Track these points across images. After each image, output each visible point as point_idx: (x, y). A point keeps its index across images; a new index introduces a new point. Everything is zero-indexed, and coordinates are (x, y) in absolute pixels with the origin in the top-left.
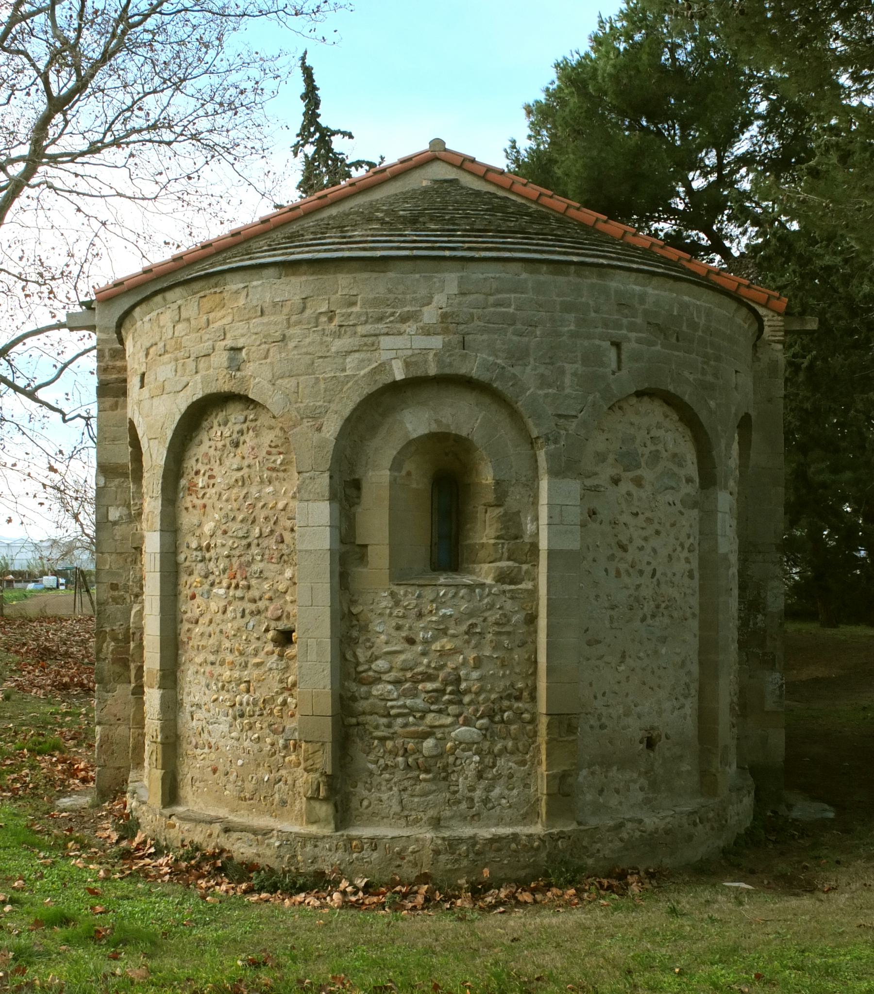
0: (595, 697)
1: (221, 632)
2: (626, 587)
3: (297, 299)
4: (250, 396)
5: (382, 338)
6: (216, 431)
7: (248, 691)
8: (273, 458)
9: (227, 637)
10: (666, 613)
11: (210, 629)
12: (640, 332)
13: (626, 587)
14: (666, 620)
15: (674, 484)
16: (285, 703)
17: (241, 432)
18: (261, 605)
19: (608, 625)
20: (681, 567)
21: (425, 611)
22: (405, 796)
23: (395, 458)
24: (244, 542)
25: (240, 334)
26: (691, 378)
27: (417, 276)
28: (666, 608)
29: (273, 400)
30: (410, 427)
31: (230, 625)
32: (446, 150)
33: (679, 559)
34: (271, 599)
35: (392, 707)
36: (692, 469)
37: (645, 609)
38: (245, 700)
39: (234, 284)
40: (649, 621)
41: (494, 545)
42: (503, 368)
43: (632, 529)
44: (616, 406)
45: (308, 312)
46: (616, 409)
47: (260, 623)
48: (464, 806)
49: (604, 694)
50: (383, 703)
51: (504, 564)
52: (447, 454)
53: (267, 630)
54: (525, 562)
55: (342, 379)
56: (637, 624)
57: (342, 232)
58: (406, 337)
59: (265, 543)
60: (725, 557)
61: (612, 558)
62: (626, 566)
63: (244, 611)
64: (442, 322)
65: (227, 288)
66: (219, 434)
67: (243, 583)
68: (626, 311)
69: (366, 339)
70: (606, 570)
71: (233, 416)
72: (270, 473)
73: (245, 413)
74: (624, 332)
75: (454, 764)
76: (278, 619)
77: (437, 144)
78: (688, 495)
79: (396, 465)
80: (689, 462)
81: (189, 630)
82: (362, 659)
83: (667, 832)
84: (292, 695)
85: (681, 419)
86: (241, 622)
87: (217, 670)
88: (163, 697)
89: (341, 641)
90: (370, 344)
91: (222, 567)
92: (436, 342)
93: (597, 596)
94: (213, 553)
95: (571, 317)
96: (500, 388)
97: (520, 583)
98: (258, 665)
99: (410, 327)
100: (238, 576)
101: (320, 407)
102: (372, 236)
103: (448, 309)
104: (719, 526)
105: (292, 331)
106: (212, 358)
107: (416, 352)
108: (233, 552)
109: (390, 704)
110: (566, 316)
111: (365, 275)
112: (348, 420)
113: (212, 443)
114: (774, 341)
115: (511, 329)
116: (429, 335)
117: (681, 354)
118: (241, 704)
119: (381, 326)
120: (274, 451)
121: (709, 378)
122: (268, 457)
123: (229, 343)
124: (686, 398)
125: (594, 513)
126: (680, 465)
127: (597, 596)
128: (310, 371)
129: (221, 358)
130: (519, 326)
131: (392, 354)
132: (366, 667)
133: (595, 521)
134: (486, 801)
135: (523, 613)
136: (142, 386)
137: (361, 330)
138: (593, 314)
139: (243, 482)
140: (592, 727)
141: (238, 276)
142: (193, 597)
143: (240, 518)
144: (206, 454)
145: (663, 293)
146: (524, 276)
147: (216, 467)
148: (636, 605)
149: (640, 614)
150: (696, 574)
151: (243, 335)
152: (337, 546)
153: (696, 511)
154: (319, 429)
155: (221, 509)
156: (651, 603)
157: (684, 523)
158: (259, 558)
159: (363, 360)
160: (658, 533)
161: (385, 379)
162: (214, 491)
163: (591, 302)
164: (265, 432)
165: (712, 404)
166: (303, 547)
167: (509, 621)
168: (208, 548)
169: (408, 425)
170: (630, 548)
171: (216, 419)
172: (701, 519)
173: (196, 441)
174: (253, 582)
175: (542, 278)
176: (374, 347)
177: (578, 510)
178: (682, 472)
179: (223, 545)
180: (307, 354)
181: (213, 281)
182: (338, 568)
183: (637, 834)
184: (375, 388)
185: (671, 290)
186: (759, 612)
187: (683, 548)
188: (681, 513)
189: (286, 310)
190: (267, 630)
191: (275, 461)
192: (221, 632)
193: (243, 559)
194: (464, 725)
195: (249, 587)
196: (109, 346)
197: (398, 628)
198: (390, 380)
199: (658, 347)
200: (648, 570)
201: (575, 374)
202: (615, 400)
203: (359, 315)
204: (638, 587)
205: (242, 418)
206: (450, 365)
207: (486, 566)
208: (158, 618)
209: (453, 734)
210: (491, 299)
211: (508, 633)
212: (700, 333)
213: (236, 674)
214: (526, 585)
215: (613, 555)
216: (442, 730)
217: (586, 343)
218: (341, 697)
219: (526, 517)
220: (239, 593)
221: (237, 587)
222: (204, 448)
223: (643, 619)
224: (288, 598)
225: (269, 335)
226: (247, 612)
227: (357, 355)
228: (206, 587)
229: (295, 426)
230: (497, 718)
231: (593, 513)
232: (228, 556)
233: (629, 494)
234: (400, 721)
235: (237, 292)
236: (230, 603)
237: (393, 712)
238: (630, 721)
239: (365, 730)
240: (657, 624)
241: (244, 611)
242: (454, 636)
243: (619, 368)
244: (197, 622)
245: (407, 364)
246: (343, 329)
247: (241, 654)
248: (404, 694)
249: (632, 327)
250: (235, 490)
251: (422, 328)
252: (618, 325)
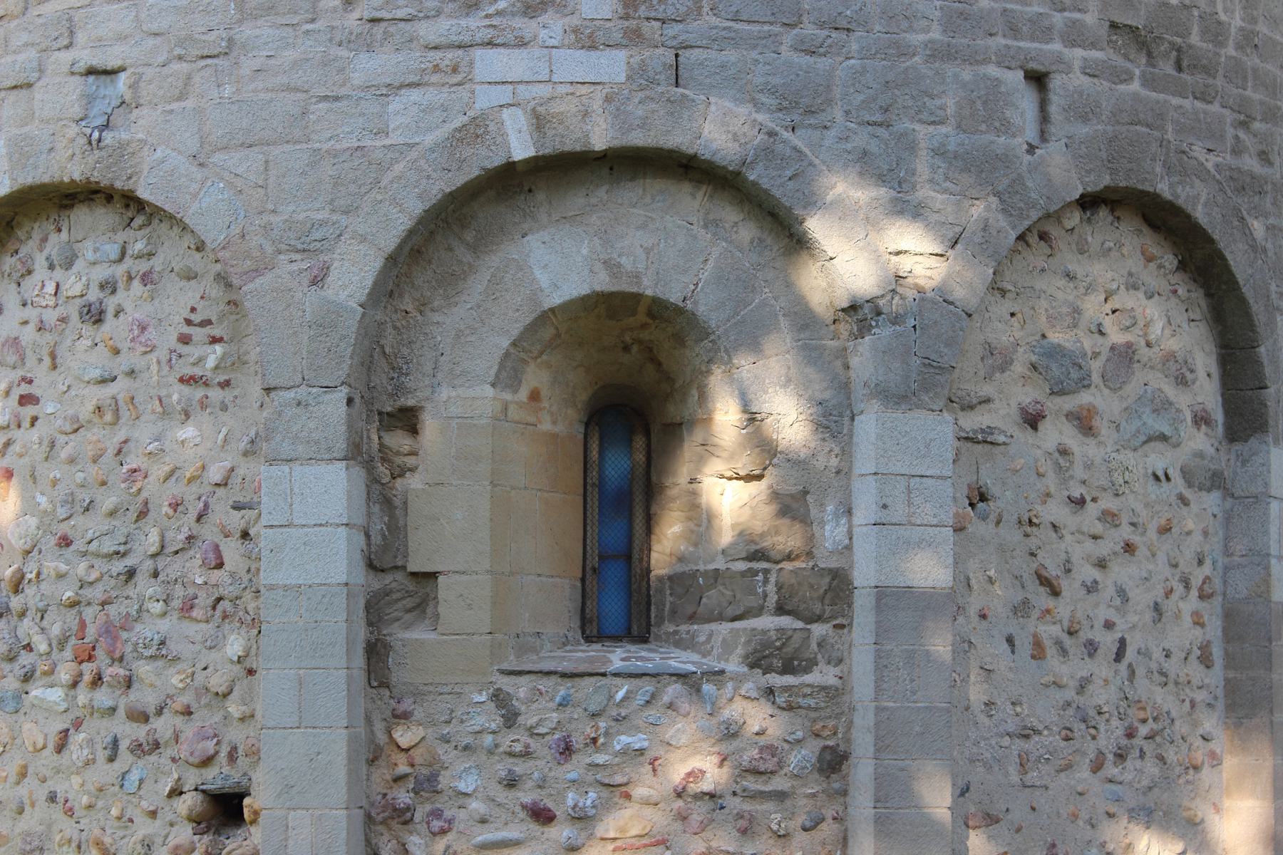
1: (52, 798)
2: (1058, 685)
4: (143, 193)
5: (478, 53)
8: (193, 351)
9: (70, 812)
10: (1148, 747)
11: (23, 791)
12: (1093, 46)
13: (1058, 685)
14: (1151, 769)
15: (1167, 430)
17: (109, 286)
18: (163, 726)
19: (1015, 778)
20: (1182, 635)
21: (577, 741)
23: (507, 355)
24: (119, 566)
26: (1211, 162)
30: (543, 279)
31: (76, 780)
33: (1178, 616)
34: (188, 712)
40: (1111, 770)
41: (743, 574)
42: (771, 134)
43: (1068, 538)
46: (1033, 239)
51: (768, 622)
52: (626, 349)
53: (176, 792)
54: (818, 619)
55: (378, 154)
56: (1083, 773)
58: (537, 52)
59: (172, 568)
62: (1055, 630)
63: (115, 742)
64: (626, 17)
66: (50, 288)
69: (437, 55)
70: (1010, 640)
71: (89, 244)
72: (186, 390)
73: (121, 236)
74: (1056, 46)
76: (207, 762)
78: (1200, 455)
80: (1201, 374)
85: (1182, 266)
86: (104, 773)
89: (368, 817)
90: (452, 61)
91: (56, 630)
92: (612, 66)
94: (31, 595)
97: (807, 670)
100: (100, 653)
101: (322, 223)
105: (247, 32)
106: (38, 93)
107: (562, 89)
108: (88, 593)
113: (30, 313)
115: (789, 38)
116: (593, 47)
117: (1187, 103)
120: (198, 334)
121: (1250, 163)
122: (184, 349)
123: (87, 57)
124: (1200, 214)
125: (983, 498)
126: (1181, 381)
128: (297, 133)
129: (60, 96)
130: (809, 30)
131: (504, 94)
135: (816, 745)
139: (109, 413)
143: (109, 502)
147: (42, 375)
148: (1079, 727)
149: (1091, 749)
150: (1217, 653)
151: (121, 38)
152: (360, 576)
153: (1216, 495)
154: (318, 281)
155: (55, 483)
156: (1115, 722)
157: (1190, 525)
158: (158, 607)
159: (429, 109)
160: (1129, 548)
162: (34, 435)
165: (1258, 227)
166: (279, 578)
169: (538, 273)
172: (1228, 519)
174: (144, 669)
176: (459, 75)
177: (947, 489)
178: (1183, 400)
179: (61, 576)
182: (362, 633)
184: (460, 180)
187: (1187, 586)
188: (1184, 501)
190: (176, 792)
191: (200, 361)
192: (52, 798)
193: (112, 610)
195: (129, 683)
198: (497, 161)
199: (1135, 86)
200: (1108, 641)
201: (939, 152)
202: (1035, 215)
205: (113, 250)
206: (644, 124)
207: (724, 628)
211: (781, 796)
214: (824, 675)
215: (1026, 602)
217: (966, 74)
221: (97, 680)
223: (1097, 767)
224: (234, 709)
225: (190, 38)
226: (124, 745)
227: (415, 95)
231: (979, 497)
232: (74, 604)
236: (78, 724)
240: (1128, 777)
241: (115, 742)
242: (647, 802)
243: (1043, 136)
245: (539, 122)
246: (379, 30)
249: (1075, 36)
251: (576, 31)
252: (1043, 32)
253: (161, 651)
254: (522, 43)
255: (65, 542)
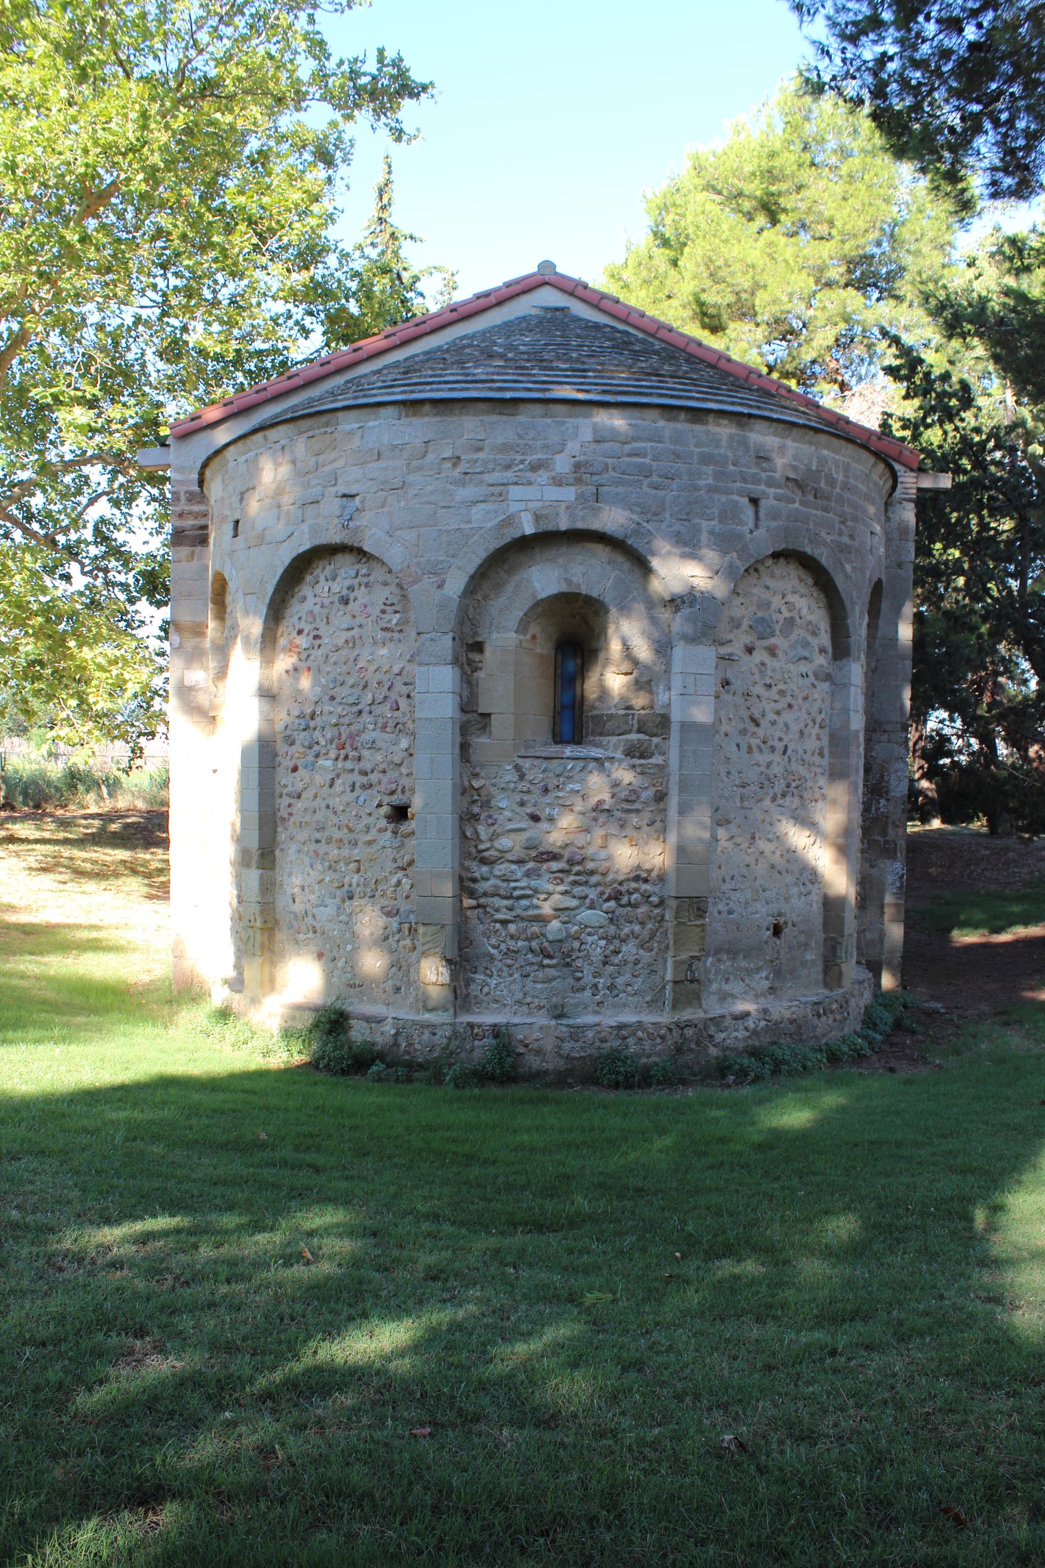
0: (724, 881)
1: (328, 807)
3: (418, 442)
4: (366, 548)
5: (511, 488)
6: (323, 587)
7: (358, 870)
8: (387, 617)
11: (315, 804)
12: (779, 487)
15: (807, 655)
16: (399, 883)
18: (374, 777)
20: (812, 744)
21: (550, 786)
22: (528, 982)
24: (355, 709)
25: (352, 479)
26: (829, 539)
27: (549, 421)
28: (796, 787)
29: (395, 555)
30: (538, 586)
31: (338, 800)
32: (556, 273)
33: (810, 735)
35: (515, 889)
36: (825, 639)
37: (776, 789)
38: (355, 881)
39: (348, 423)
42: (638, 524)
44: (753, 569)
45: (431, 457)
46: (751, 571)
47: (372, 797)
48: (588, 993)
49: (732, 878)
50: (505, 885)
51: (634, 737)
53: (379, 806)
54: (655, 735)
57: (463, 368)
59: (378, 710)
60: (856, 734)
61: (743, 732)
65: (340, 428)
67: (352, 754)
68: (765, 465)
70: (738, 745)
73: (356, 567)
74: (763, 487)
75: (579, 950)
76: (392, 793)
77: (547, 265)
78: (821, 666)
79: (522, 627)
80: (823, 631)
81: (290, 806)
82: (483, 836)
83: (792, 1021)
84: (406, 876)
85: (816, 584)
86: (350, 797)
87: (322, 848)
88: (261, 877)
91: (329, 736)
92: (569, 493)
93: (728, 773)
95: (709, 470)
96: (635, 545)
97: (650, 757)
98: (370, 843)
99: (542, 476)
100: (347, 746)
102: (498, 374)
103: (583, 458)
104: (852, 699)
105: (411, 478)
106: (322, 505)
108: (342, 720)
109: (513, 884)
110: (704, 468)
111: (494, 418)
112: (472, 577)
114: (905, 500)
115: (646, 482)
116: (561, 485)
117: (819, 513)
118: (350, 885)
119: (509, 475)
120: (389, 609)
121: (846, 539)
123: (342, 489)
124: (824, 561)
125: (728, 684)
127: (728, 773)
129: (331, 506)
130: (655, 478)
131: (522, 506)
132: (488, 845)
133: (728, 692)
134: (611, 987)
136: (235, 536)
137: (489, 478)
138: (732, 468)
140: (719, 912)
141: (353, 414)
142: (295, 769)
144: (311, 613)
145: (802, 446)
146: (661, 423)
147: (322, 626)
149: (771, 792)
151: (357, 481)
152: (458, 714)
158: (372, 727)
160: (790, 706)
161: (512, 534)
162: (319, 652)
163: (729, 454)
164: (378, 588)
166: (423, 715)
167: (638, 798)
168: (313, 717)
170: (762, 722)
171: (322, 571)
173: (298, 596)
174: (366, 753)
175: (679, 426)
176: (502, 497)
179: (331, 713)
180: (428, 503)
181: (324, 419)
183: (763, 1023)
184: (502, 543)
185: (810, 443)
186: (882, 797)
188: (814, 686)
189: (406, 455)
190: (379, 806)
191: (390, 621)
192: (328, 807)
194: (590, 908)
196: (185, 488)
197: (522, 804)
198: (518, 535)
199: (797, 505)
200: (780, 746)
201: (711, 533)
202: (752, 561)
203: (486, 462)
204: (769, 765)
205: (353, 573)
207: (614, 739)
208: (256, 792)
209: (578, 917)
210: (627, 448)
212: (838, 490)
213: (346, 852)
216: (567, 913)
217: (724, 498)
218: (461, 879)
219: (658, 686)
220: (349, 765)
221: (346, 758)
222: (308, 605)
224: (404, 770)
226: (357, 785)
227: (483, 506)
228: (310, 758)
229: (414, 582)
230: (625, 900)
231: (726, 683)
233: (763, 664)
234: (524, 902)
235: (351, 433)
236: (338, 776)
237: (516, 893)
238: (758, 906)
239: (486, 913)
243: (757, 526)
244: (299, 797)
245: (537, 518)
246: (468, 477)
247: (350, 830)
248: (528, 874)
249: (771, 483)
250: (344, 652)
251: (553, 478)
252: (757, 481)
253: (373, 746)
254: (530, 483)
255: (333, 698)
